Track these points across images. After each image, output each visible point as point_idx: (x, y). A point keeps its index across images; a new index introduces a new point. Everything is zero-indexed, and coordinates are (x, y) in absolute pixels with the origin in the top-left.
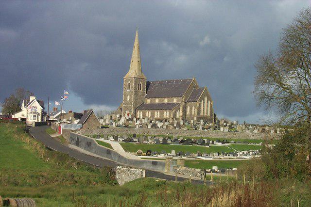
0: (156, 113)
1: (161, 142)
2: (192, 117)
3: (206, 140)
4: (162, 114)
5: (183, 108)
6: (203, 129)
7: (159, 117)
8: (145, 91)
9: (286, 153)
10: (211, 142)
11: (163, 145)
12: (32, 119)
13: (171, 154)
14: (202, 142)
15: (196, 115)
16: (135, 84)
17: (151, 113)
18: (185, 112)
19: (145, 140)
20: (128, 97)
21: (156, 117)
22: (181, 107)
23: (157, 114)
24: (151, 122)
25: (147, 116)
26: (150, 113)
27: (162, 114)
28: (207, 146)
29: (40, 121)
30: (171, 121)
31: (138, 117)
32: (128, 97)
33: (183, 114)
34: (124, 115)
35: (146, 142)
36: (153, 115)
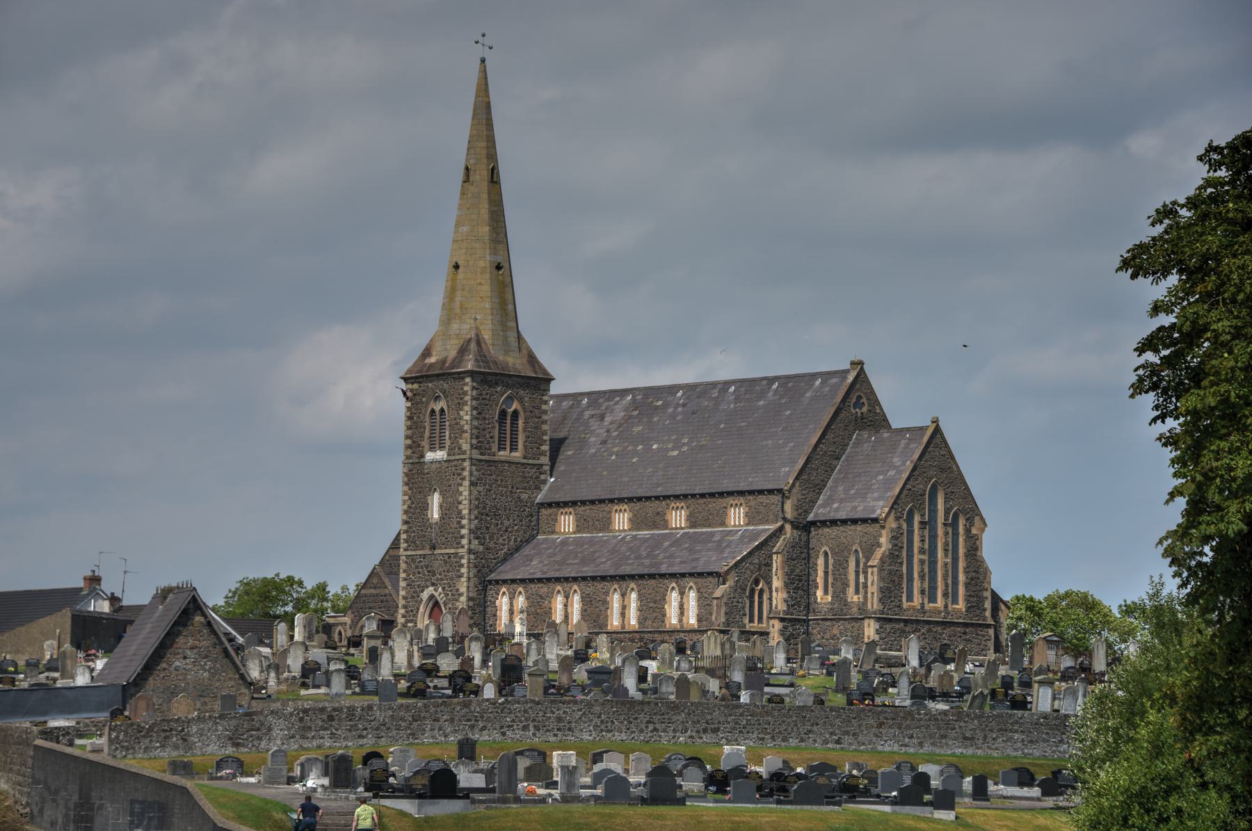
0: (674, 596)
3: (931, 769)
4: (653, 608)
5: (789, 560)
6: (921, 694)
7: (633, 621)
8: (545, 460)
10: (967, 783)
11: (607, 809)
14: (907, 781)
15: (874, 604)
16: (479, 413)
17: (585, 600)
18: (800, 585)
20: (436, 499)
21: (615, 622)
22: (777, 561)
25: (558, 617)
27: (653, 608)
32: (436, 499)
33: (792, 604)
34: (411, 614)
35: (542, 791)
36: (595, 613)
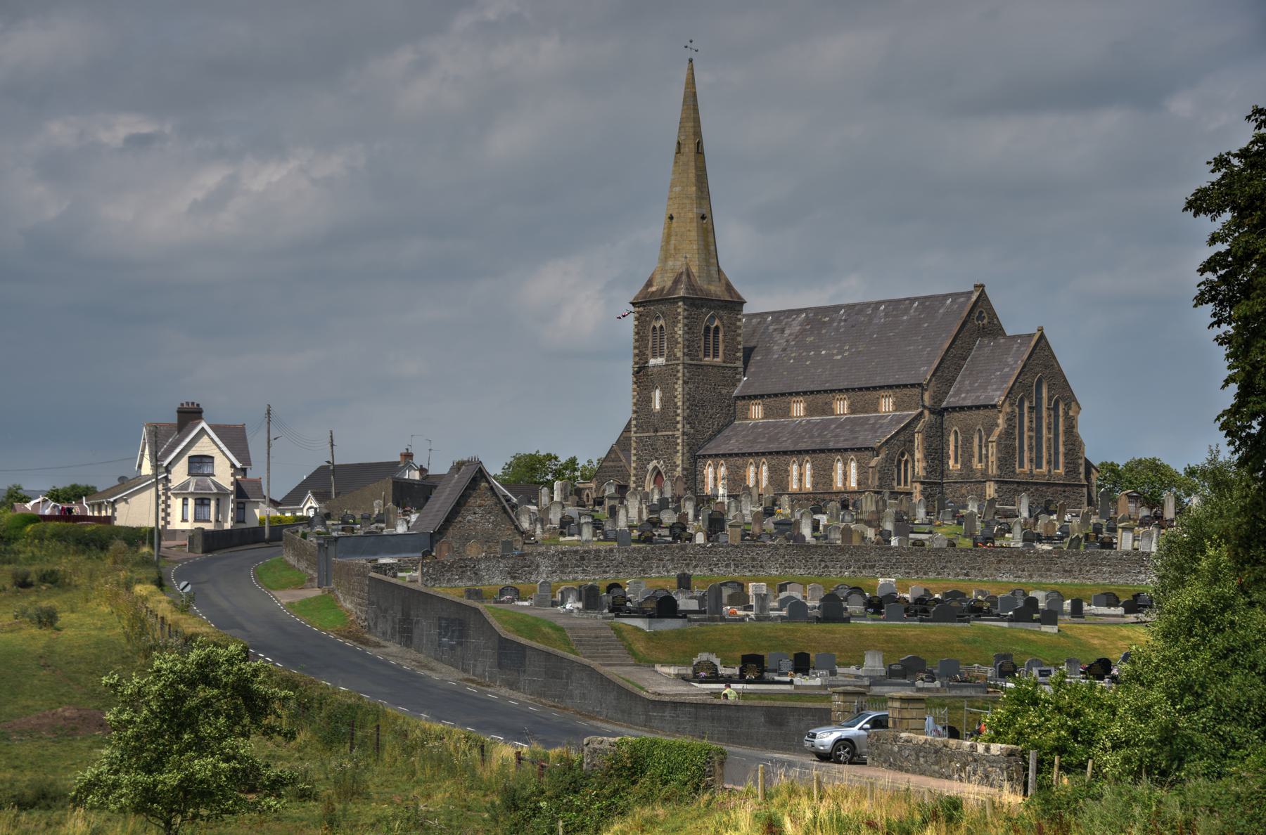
1: (816, 613)
2: (973, 481)
3: (1040, 595)
7: (808, 485)
8: (739, 364)
9: (1200, 691)
10: (1067, 605)
11: (790, 626)
12: (190, 516)
13: (860, 672)
14: (1021, 604)
16: (689, 328)
17: (772, 470)
18: (936, 456)
19: (733, 600)
21: (794, 486)
22: (918, 439)
23: (801, 477)
24: (769, 512)
26: (853, 466)
27: (824, 475)
28: (1046, 628)
29: (228, 525)
30: (868, 505)
31: (708, 489)
32: (657, 394)
33: (930, 470)
36: (779, 479)
